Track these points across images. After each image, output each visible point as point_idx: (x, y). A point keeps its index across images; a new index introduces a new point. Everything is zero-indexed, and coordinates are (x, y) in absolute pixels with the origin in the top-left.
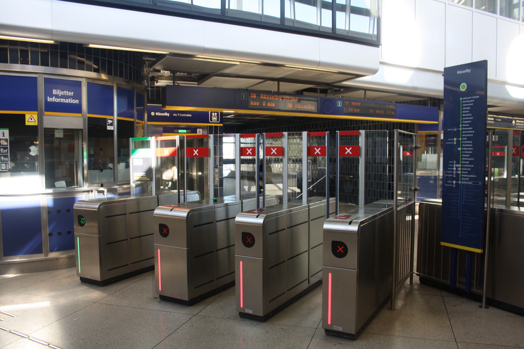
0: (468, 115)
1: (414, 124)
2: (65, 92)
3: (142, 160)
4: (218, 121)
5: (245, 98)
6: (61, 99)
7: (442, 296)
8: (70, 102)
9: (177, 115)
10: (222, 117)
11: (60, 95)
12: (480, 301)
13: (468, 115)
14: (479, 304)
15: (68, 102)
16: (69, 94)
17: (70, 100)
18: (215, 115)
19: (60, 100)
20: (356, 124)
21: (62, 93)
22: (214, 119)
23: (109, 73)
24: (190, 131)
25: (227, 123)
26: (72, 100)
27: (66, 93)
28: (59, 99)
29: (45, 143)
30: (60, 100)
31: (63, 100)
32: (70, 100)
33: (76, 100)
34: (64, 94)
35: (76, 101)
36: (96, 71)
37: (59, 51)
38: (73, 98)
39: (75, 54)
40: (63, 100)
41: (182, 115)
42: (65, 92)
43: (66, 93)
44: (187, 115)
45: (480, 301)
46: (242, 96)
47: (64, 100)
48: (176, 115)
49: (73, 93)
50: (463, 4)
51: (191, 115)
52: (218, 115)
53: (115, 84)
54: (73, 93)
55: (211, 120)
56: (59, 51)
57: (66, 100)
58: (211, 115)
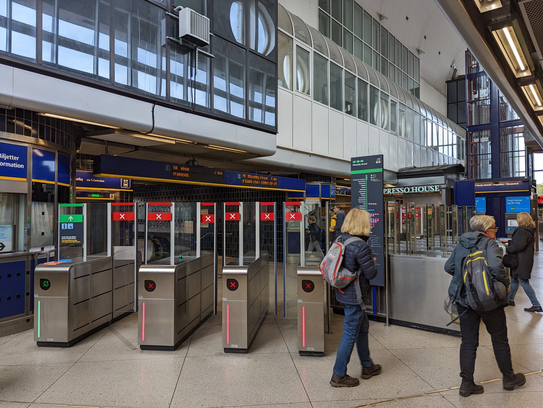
0: (362, 194)
1: (285, 192)
2: (10, 156)
3: (72, 225)
4: (129, 187)
5: (169, 169)
6: (6, 164)
7: (519, 151)
8: (15, 167)
9: (91, 180)
10: (133, 184)
11: (5, 159)
12: (385, 322)
13: (362, 194)
14: (385, 324)
15: (13, 166)
16: (14, 158)
17: (15, 164)
18: (126, 182)
19: (5, 164)
20: (236, 191)
21: (7, 157)
22: (126, 185)
23: (46, 139)
24: (103, 196)
25: (98, 181)
26: (18, 164)
27: (11, 158)
28: (4, 163)
29: (300, 233)
30: (5, 164)
31: (8, 164)
32: (15, 164)
33: (21, 165)
34: (9, 158)
35: (22, 166)
36: (35, 136)
37: (6, 115)
38: (19, 162)
39: (22, 121)
40: (8, 164)
41: (95, 181)
42: (10, 156)
43: (11, 158)
44: (100, 181)
45: (385, 322)
46: (167, 167)
47: (10, 164)
48: (90, 180)
49: (18, 158)
50: (385, 129)
51: (104, 181)
52: (129, 182)
53: (57, 151)
54: (18, 158)
55: (123, 186)
56: (6, 115)
57: (11, 165)
58: (123, 182)
